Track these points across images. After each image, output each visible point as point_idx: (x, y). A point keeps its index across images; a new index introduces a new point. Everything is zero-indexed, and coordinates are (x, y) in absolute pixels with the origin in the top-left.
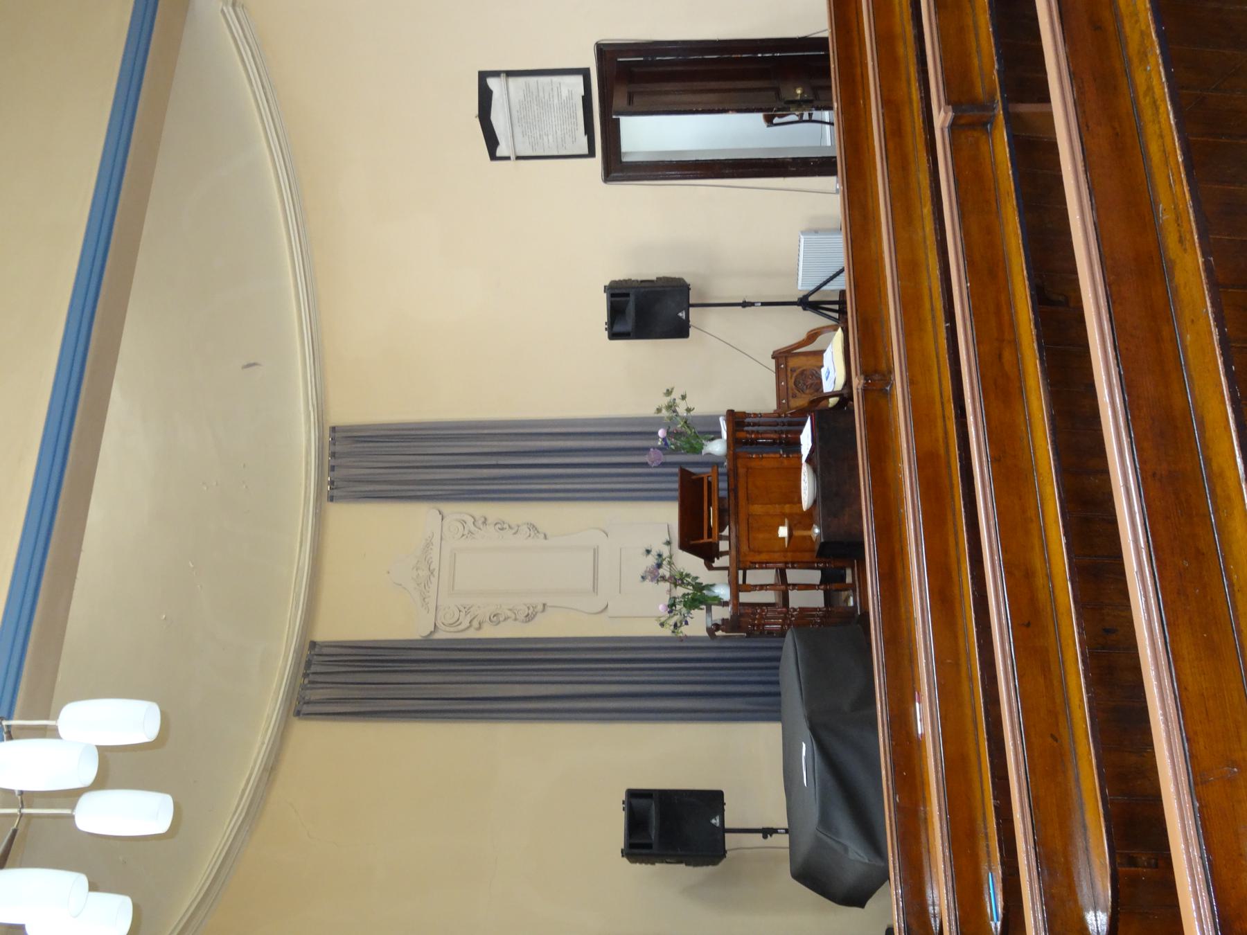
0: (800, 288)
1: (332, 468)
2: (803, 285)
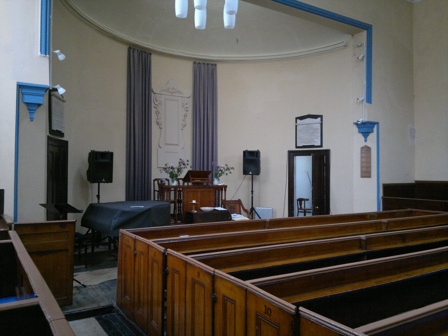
0: (256, 208)
1: (204, 64)
2: (257, 208)
